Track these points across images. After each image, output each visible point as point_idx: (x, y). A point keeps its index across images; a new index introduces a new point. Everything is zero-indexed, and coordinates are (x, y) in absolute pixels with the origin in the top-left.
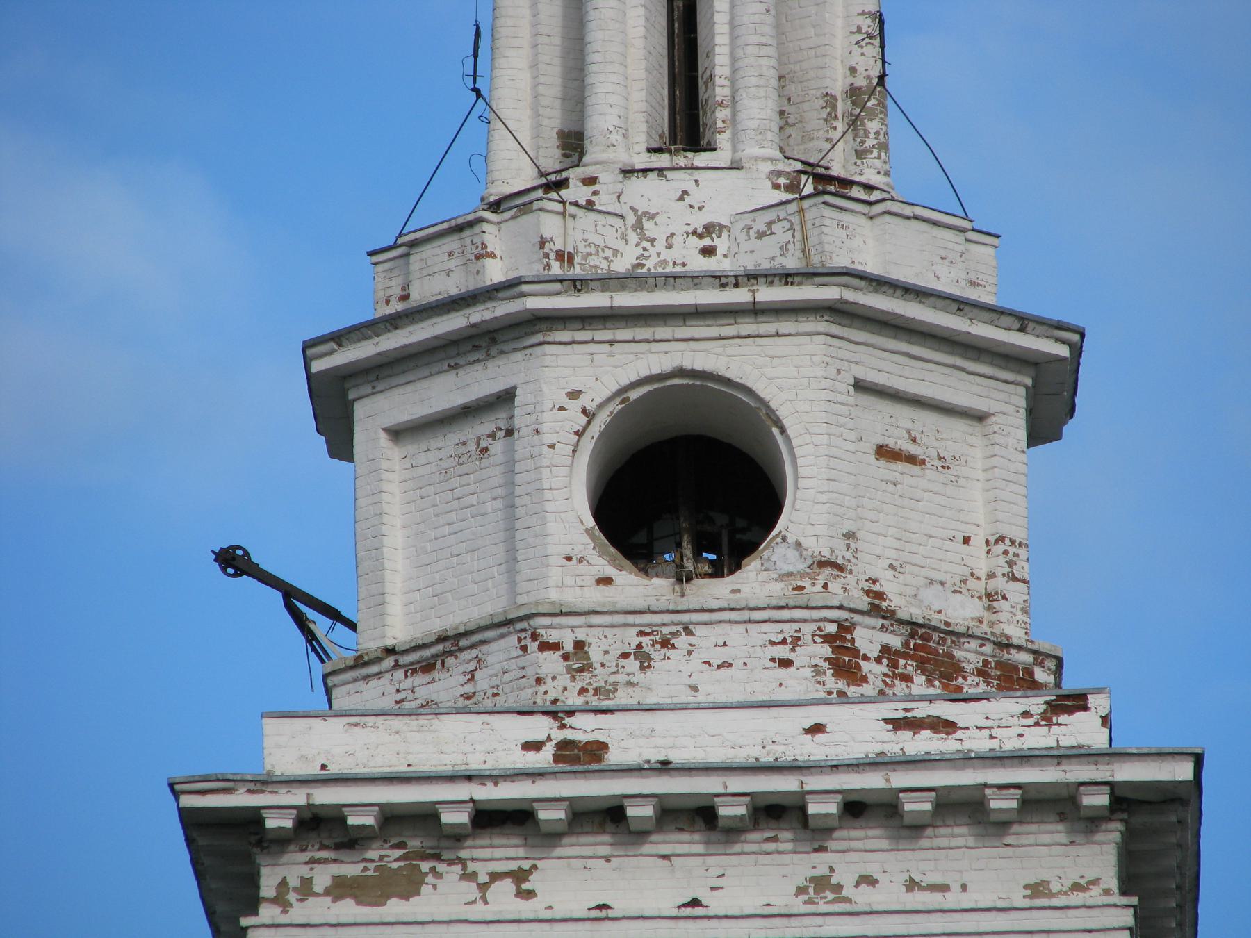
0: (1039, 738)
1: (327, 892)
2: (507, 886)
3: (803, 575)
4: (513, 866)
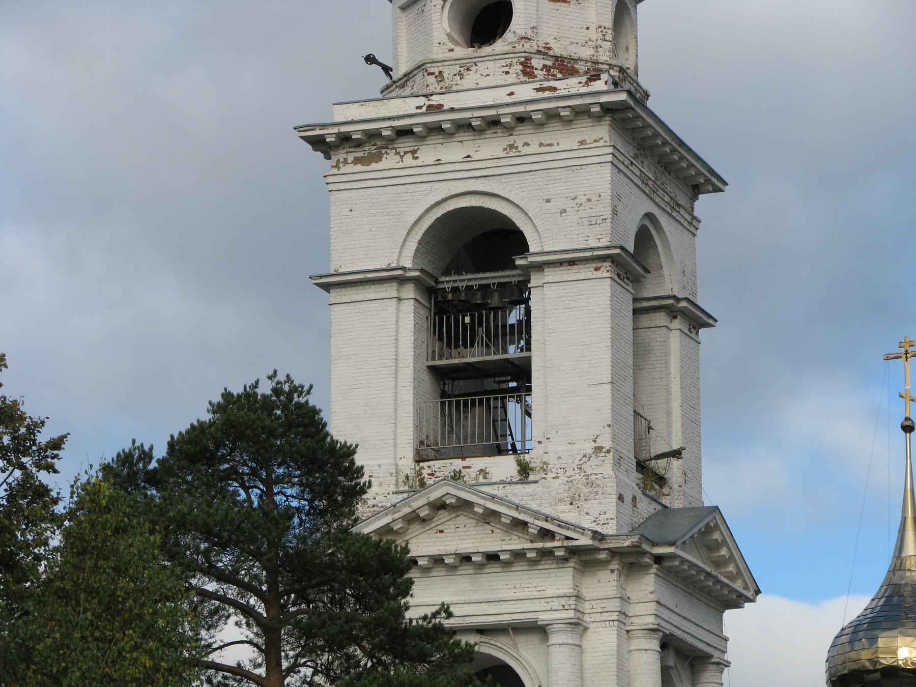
0: (584, 90)
1: (352, 162)
2: (410, 155)
3: (516, 42)
4: (412, 149)
